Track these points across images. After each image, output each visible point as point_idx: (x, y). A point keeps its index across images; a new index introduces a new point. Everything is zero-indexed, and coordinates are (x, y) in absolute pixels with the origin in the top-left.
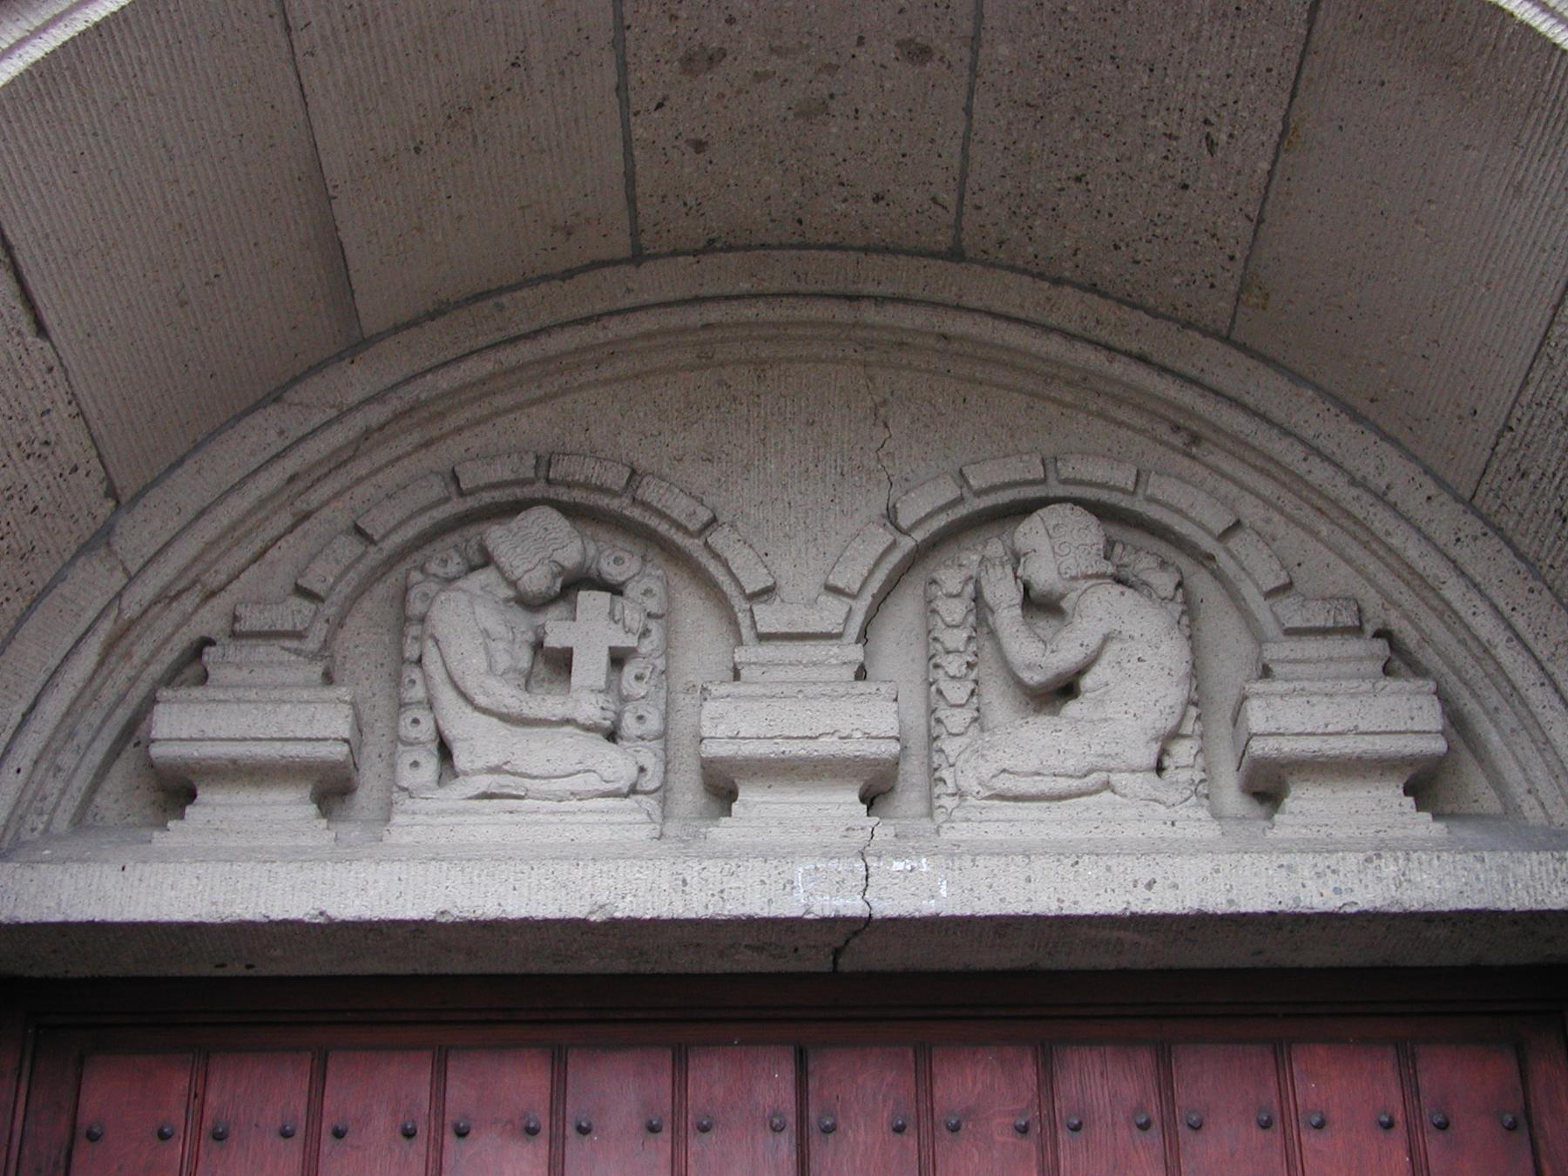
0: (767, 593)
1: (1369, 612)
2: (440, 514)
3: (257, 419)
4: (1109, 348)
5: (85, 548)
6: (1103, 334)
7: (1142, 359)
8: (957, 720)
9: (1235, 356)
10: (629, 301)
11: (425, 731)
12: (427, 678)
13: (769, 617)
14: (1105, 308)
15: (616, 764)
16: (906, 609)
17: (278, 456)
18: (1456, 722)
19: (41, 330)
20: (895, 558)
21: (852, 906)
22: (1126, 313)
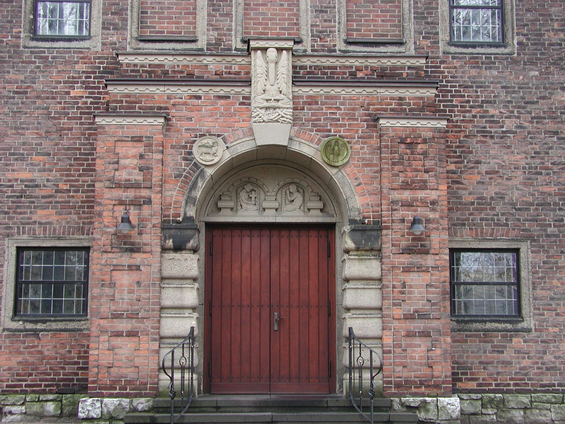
0: (268, 192)
2: (353, 363)
8: (283, 203)
13: (268, 194)
15: (255, 208)
16: (280, 192)
18: (324, 206)
21: (274, 221)
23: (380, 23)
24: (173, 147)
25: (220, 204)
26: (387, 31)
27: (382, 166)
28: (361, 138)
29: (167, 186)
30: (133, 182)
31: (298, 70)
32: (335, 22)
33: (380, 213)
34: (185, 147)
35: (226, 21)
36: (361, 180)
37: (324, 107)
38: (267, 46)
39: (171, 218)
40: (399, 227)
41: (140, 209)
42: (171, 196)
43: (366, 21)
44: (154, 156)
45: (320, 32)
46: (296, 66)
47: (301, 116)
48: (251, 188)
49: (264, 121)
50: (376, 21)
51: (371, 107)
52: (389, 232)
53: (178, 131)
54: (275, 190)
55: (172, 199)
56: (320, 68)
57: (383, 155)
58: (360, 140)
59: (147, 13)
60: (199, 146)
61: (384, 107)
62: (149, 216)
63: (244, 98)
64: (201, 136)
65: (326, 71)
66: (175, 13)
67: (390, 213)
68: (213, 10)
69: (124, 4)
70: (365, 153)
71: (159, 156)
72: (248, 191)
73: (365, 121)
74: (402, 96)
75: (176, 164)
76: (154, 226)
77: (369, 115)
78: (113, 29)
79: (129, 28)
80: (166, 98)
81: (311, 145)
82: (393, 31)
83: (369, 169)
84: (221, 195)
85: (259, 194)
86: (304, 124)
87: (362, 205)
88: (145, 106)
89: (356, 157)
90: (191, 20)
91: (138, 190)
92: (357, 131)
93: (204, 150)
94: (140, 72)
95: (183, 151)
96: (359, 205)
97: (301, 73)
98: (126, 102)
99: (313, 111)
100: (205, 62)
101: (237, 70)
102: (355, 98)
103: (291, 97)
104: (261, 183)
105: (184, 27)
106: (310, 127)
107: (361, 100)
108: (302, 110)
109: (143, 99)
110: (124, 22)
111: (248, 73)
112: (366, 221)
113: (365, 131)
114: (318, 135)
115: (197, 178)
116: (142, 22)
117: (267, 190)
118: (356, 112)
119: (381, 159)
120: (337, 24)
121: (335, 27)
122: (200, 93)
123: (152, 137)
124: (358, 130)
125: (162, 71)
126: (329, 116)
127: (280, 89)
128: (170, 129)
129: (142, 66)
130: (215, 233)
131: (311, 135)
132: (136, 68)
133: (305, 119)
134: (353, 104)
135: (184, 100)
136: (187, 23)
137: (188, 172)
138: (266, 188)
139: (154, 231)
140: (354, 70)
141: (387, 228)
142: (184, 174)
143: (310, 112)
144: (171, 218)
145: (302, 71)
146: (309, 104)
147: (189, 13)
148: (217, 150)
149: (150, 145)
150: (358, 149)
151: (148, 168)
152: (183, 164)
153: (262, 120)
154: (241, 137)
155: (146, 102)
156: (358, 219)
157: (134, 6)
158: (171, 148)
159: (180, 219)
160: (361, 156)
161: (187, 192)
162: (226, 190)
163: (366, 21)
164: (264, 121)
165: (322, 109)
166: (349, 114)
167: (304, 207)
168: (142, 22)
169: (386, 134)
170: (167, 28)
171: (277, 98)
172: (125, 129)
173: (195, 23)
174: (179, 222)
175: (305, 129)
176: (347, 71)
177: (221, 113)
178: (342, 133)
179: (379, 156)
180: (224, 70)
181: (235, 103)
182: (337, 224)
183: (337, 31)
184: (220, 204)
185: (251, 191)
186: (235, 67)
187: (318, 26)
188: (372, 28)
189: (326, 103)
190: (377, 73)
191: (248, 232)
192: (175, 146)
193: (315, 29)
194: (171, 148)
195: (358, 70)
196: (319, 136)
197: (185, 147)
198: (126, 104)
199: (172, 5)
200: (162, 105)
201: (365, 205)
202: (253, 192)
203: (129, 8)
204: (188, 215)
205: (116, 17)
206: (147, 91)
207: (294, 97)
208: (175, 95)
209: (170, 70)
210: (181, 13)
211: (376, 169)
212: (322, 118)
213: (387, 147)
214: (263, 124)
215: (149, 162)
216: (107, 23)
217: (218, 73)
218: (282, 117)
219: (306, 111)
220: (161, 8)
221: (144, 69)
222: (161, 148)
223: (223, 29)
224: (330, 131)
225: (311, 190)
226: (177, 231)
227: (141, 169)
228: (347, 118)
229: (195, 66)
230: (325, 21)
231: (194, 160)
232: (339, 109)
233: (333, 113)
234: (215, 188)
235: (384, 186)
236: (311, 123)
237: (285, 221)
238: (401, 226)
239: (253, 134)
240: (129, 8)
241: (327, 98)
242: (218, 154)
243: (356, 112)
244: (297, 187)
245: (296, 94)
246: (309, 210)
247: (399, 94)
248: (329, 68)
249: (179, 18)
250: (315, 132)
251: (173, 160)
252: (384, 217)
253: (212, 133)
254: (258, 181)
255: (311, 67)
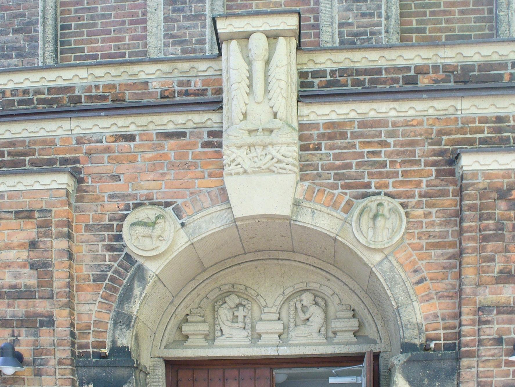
0: (265, 306)
1: (352, 306)
3: (191, 282)
4: (316, 267)
5: (170, 304)
6: (315, 265)
7: (321, 269)
9: (335, 268)
10: (244, 261)
11: (219, 328)
12: (218, 321)
13: (266, 310)
14: (316, 260)
15: (245, 333)
16: (286, 307)
17: (195, 288)
19: (165, 286)
20: (284, 299)
21: (276, 353)
22: (319, 261)
23: (457, 16)
24: (88, 228)
25: (186, 329)
26: (470, 29)
27: (464, 245)
28: (424, 196)
29: (81, 296)
30: (23, 289)
31: (310, 79)
32: (380, 15)
33: (457, 330)
34: (109, 228)
35: (196, 26)
36: (425, 274)
37: (357, 141)
38: (248, 28)
39: (91, 350)
40: (492, 352)
41: (36, 335)
42: (90, 313)
43: (432, 13)
44: (54, 244)
45: (355, 35)
46: (307, 73)
47: (315, 161)
48: (237, 301)
49: (245, 172)
50: (450, 13)
51: (445, 138)
52: (473, 361)
53: (97, 199)
54: (277, 303)
55: (90, 319)
56: (350, 73)
57: (465, 224)
58: (424, 199)
59: (69, 27)
60: (133, 225)
61: (469, 136)
62: (50, 345)
63: (211, 134)
64: (137, 206)
65: (361, 78)
66: (114, 24)
67: (476, 328)
68: (174, 11)
69: (33, 15)
70: (432, 224)
71: (63, 244)
72: (233, 306)
73: (434, 164)
74: (502, 115)
75: (96, 258)
76: (60, 363)
77: (441, 153)
78: (16, 57)
79: (40, 52)
80: (74, 142)
81: (335, 214)
82: (481, 29)
83: (439, 251)
84: (188, 315)
85: (251, 310)
86: (320, 175)
87: (426, 318)
88: (39, 159)
89: (417, 231)
90: (140, 33)
91: (31, 302)
92: (418, 184)
93: (140, 230)
94: (33, 104)
95: (106, 234)
96: (419, 318)
97: (316, 84)
98: (9, 154)
99: (337, 151)
100: (143, 76)
101: (199, 86)
102: (415, 123)
103: (295, 124)
104: (253, 292)
105: (128, 44)
106: (331, 181)
107: (426, 126)
108: (316, 149)
109: (37, 148)
110: (34, 44)
111: (219, 91)
112: (432, 345)
113: (434, 183)
114: (346, 194)
115: (131, 281)
116: (62, 43)
117: (264, 304)
118: (418, 150)
119: (461, 232)
120: (383, 19)
121: (379, 24)
122: (132, 129)
123: (50, 211)
124: (420, 182)
125: (70, 97)
126: (366, 159)
127: (275, 110)
128: (82, 197)
129: (38, 92)
130: (182, 374)
131: (334, 194)
132: (26, 97)
133: (322, 166)
134: (413, 134)
135: (105, 144)
136: (133, 38)
137: (116, 272)
138: (262, 301)
139: (61, 371)
140: (412, 73)
141: (470, 355)
142: (110, 274)
143: (331, 152)
144: (91, 350)
145: (317, 81)
146: (330, 139)
147: (137, 22)
148: (164, 231)
149: (45, 225)
150: (419, 216)
151: (45, 265)
152: (107, 258)
153: (241, 170)
154: (206, 205)
155: (42, 152)
156: (417, 342)
157: (48, 17)
158: (86, 231)
159: (106, 351)
160: (424, 229)
161: (114, 305)
162: (196, 306)
163: (432, 13)
164: (245, 172)
165: (354, 146)
166: (404, 152)
167: (326, 328)
168: (62, 43)
169: (473, 184)
170: (101, 49)
171: (270, 126)
172: (6, 200)
173: (145, 37)
174: (106, 357)
175: (321, 185)
176: (400, 76)
177: (170, 163)
178: (391, 189)
179: (457, 228)
180: (177, 88)
181: (195, 145)
182: (381, 355)
183: (383, 31)
184: (186, 329)
185: (238, 306)
186: (196, 83)
187: (351, 25)
188: (444, 25)
189: (361, 135)
190: (455, 76)
191: (234, 373)
192: (92, 226)
193: (345, 30)
194: (86, 231)
195: (421, 73)
196: (347, 198)
197: (109, 228)
198: (9, 158)
199: (109, 10)
200: (68, 156)
201: (431, 317)
202: (241, 308)
203: (40, 20)
204: (119, 344)
205: (20, 36)
206: (42, 133)
207: (302, 127)
208: (89, 136)
209: (83, 95)
210: (123, 23)
211: (451, 251)
212: (354, 162)
213: (472, 208)
214: (244, 177)
215: (46, 254)
216: (7, 47)
217: (166, 94)
218: (279, 161)
219: (323, 151)
220: (92, 18)
221: (39, 96)
222: (66, 229)
223: (190, 41)
224: (368, 186)
225: (338, 301)
226: (99, 370)
227: (33, 266)
228: (399, 160)
229: (126, 85)
230: (364, 15)
231: (126, 251)
232: (385, 144)
233: (373, 153)
234: (177, 302)
235: (465, 281)
236: (333, 172)
237: (294, 353)
238: (494, 350)
239: (227, 200)
240: (40, 20)
241: (363, 124)
242: (165, 235)
243: (418, 150)
244: (315, 296)
245: (305, 121)
246: (335, 333)
247: (496, 110)
248: (366, 72)
249: (120, 31)
250: (340, 190)
251: (90, 251)
252: (465, 336)
253: (155, 200)
254: (249, 290)
255: (333, 72)
